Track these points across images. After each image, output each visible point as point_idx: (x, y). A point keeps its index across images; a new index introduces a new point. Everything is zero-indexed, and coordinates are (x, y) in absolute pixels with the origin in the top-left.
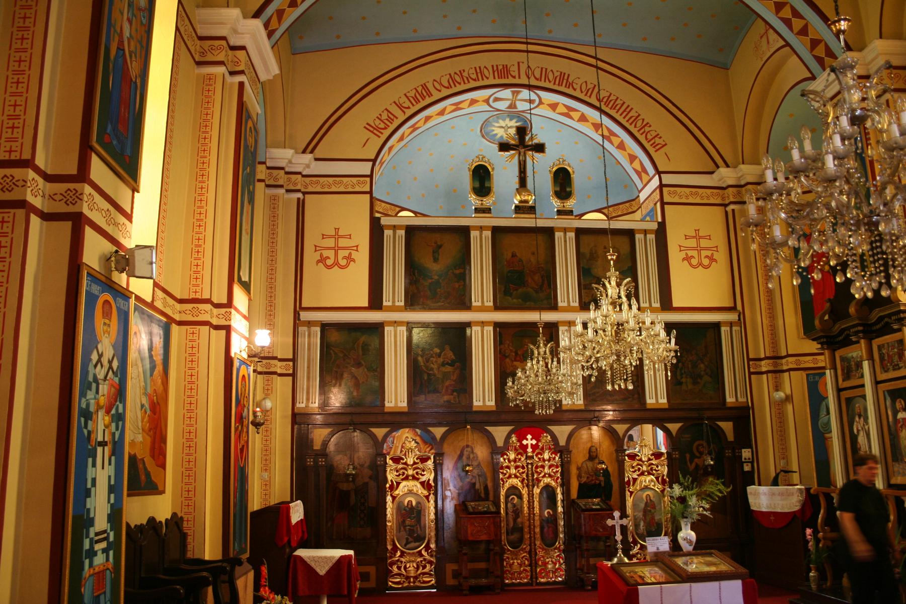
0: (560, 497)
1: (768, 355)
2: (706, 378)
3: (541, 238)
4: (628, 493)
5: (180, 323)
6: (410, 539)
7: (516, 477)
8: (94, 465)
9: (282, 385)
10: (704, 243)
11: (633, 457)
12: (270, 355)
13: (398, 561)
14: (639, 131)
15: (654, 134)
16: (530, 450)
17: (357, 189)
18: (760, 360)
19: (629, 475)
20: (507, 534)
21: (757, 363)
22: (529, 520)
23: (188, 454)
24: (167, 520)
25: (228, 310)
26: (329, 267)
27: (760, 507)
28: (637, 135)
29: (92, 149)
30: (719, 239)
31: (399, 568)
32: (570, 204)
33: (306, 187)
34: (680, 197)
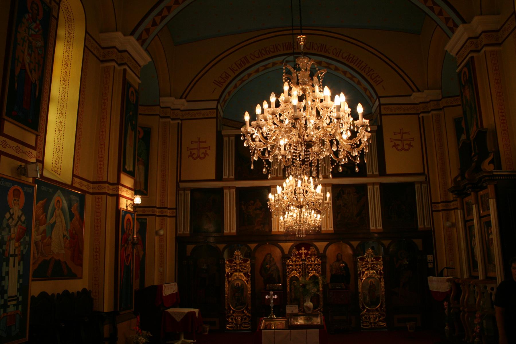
1: (442, 200)
5: (92, 194)
7: (296, 270)
8: (7, 265)
9: (170, 222)
13: (231, 315)
16: (303, 256)
17: (210, 116)
18: (438, 203)
21: (437, 205)
26: (194, 159)
28: (366, 76)
29: (4, 119)
31: (232, 319)
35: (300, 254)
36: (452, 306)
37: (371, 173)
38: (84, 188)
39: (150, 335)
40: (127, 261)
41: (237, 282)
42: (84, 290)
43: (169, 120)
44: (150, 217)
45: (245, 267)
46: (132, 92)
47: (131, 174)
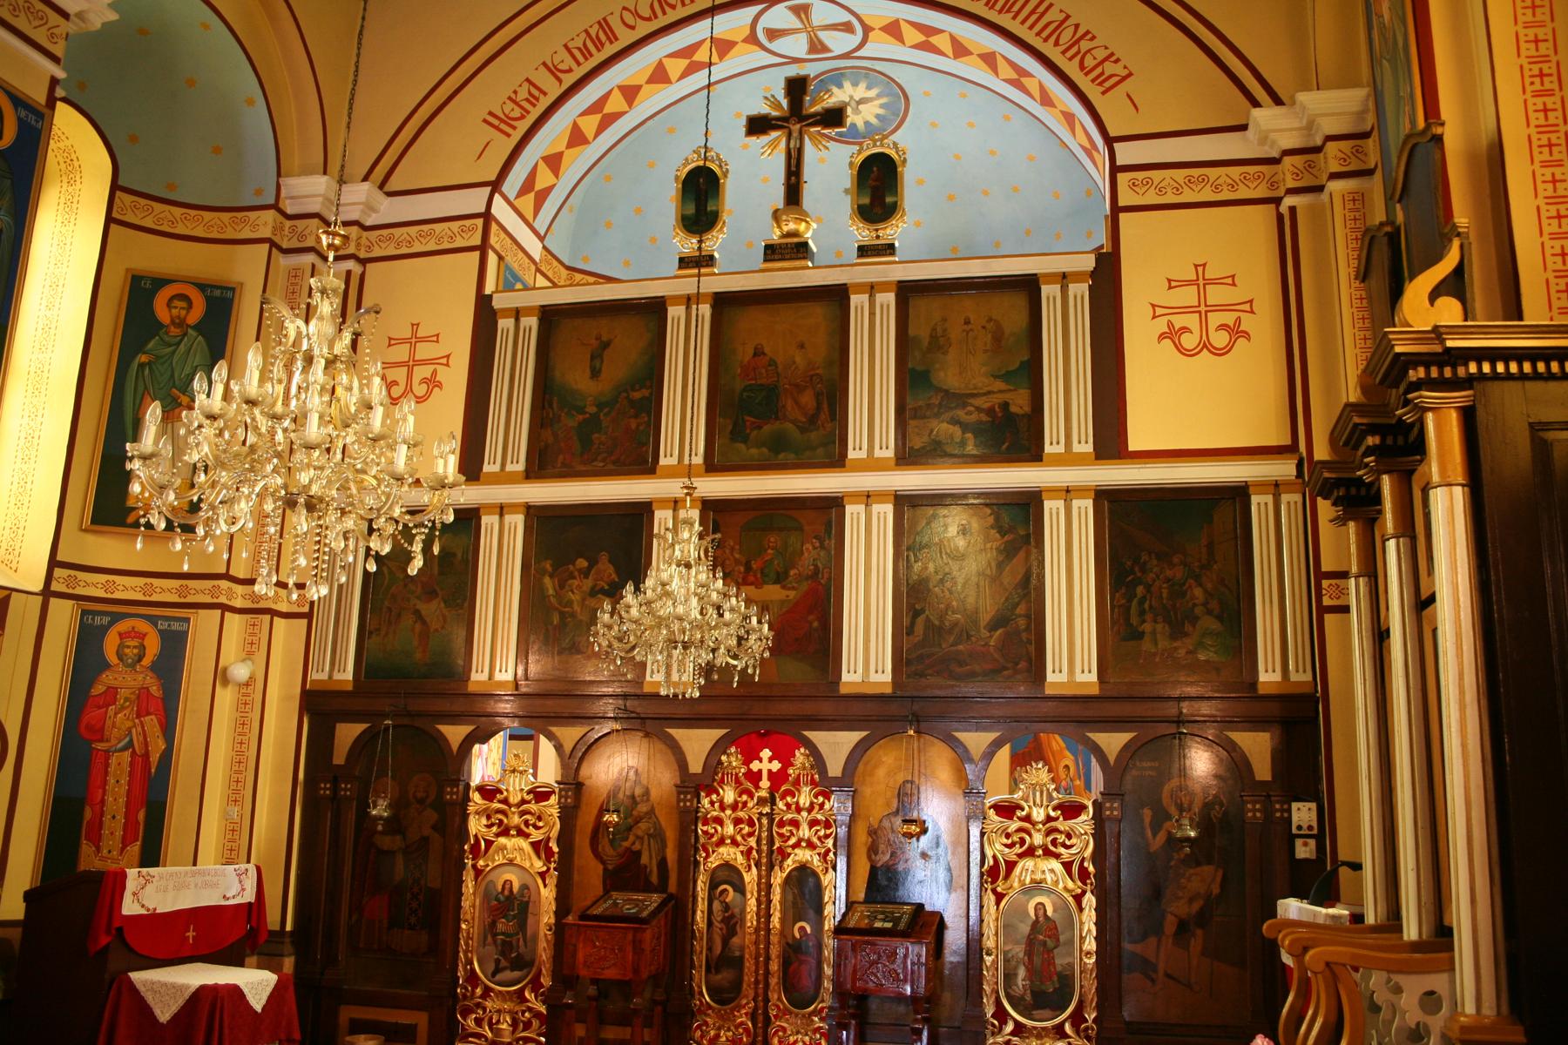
3: (818, 314)
6: (503, 963)
10: (1215, 295)
15: (1101, 54)
16: (765, 783)
17: (460, 243)
20: (708, 970)
22: (756, 943)
31: (478, 1022)
34: (1161, 191)
35: (755, 777)
45: (539, 818)
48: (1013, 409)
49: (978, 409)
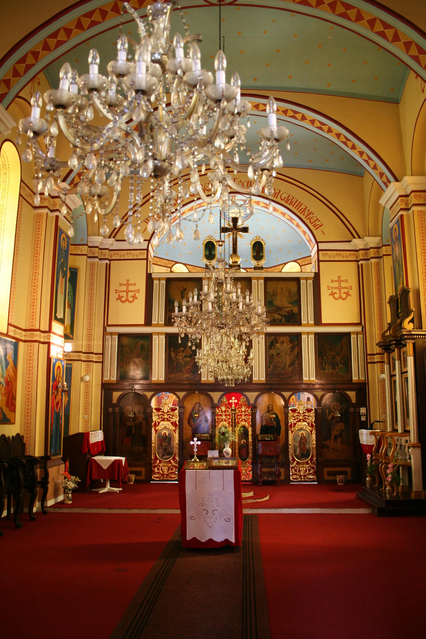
0: (250, 433)
1: (378, 352)
2: (341, 366)
4: (290, 432)
5: (25, 341)
6: (165, 454)
7: (225, 421)
9: (96, 368)
10: (343, 284)
11: (294, 411)
12: (90, 351)
13: (158, 465)
14: (306, 217)
15: (315, 219)
16: (233, 406)
17: (140, 257)
18: (374, 355)
19: (291, 421)
21: (372, 356)
23: (27, 406)
24: (13, 436)
25: (49, 334)
27: (363, 442)
28: (305, 220)
30: (353, 282)
31: (158, 469)
32: (262, 263)
33: (111, 256)
36: (373, 458)
37: (306, 322)
38: (18, 336)
39: (78, 480)
40: (57, 408)
41: (164, 431)
42: (18, 435)
43: (97, 260)
44: (75, 362)
46: (64, 238)
47: (62, 321)
48: (294, 312)
49: (285, 311)
